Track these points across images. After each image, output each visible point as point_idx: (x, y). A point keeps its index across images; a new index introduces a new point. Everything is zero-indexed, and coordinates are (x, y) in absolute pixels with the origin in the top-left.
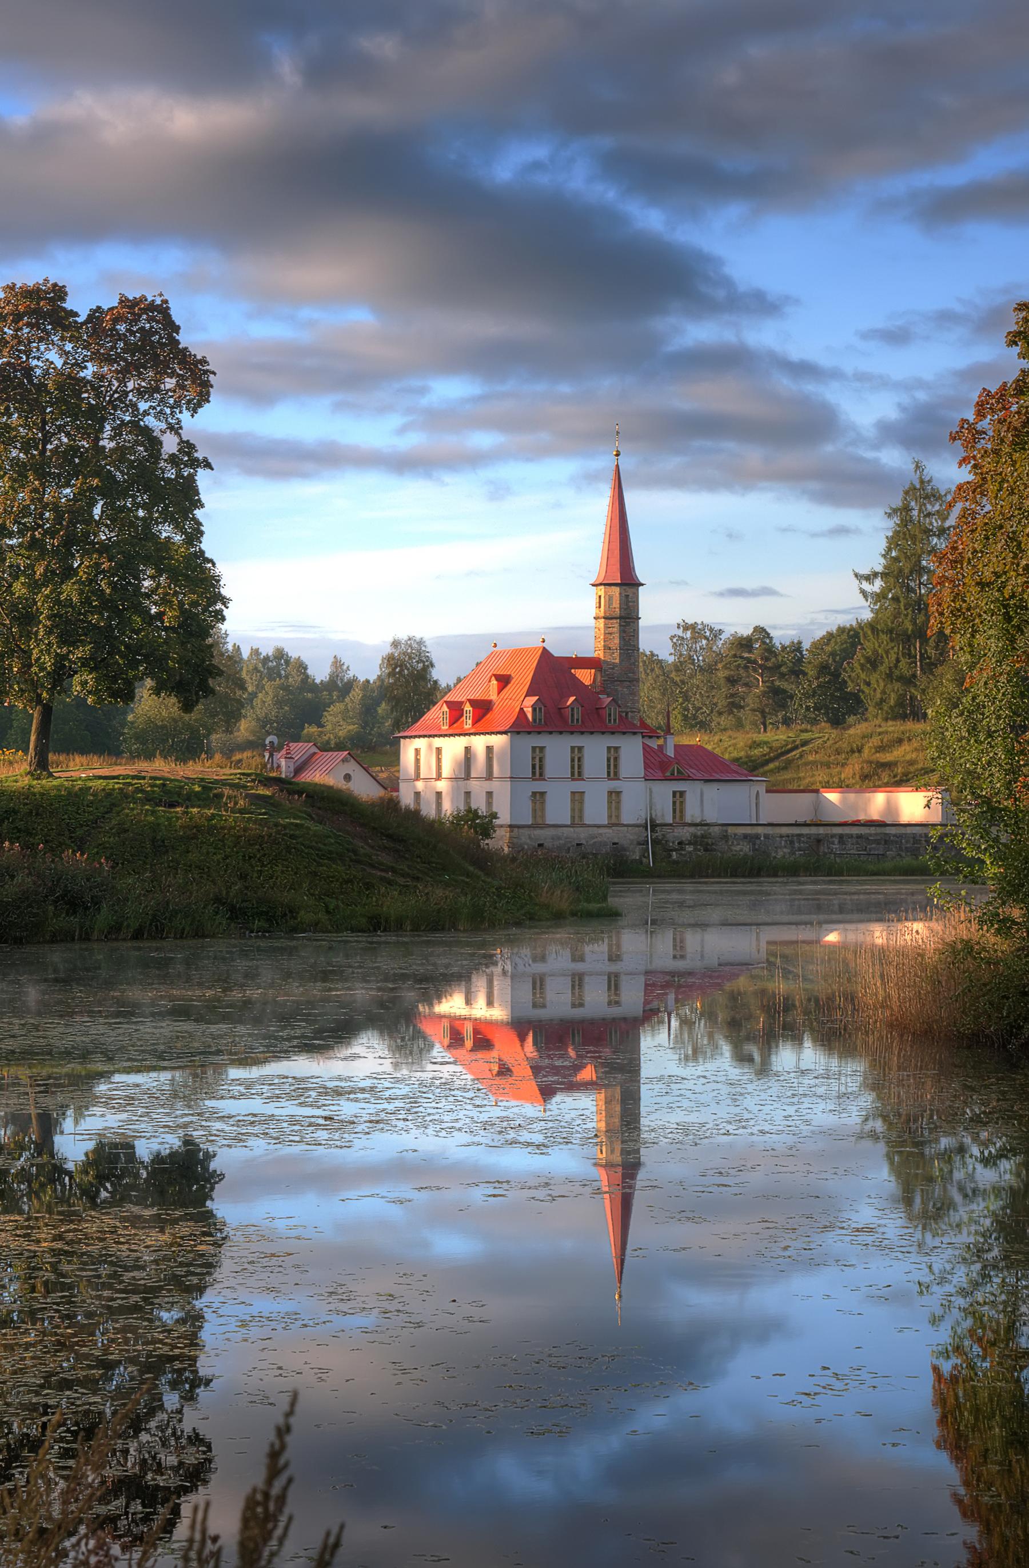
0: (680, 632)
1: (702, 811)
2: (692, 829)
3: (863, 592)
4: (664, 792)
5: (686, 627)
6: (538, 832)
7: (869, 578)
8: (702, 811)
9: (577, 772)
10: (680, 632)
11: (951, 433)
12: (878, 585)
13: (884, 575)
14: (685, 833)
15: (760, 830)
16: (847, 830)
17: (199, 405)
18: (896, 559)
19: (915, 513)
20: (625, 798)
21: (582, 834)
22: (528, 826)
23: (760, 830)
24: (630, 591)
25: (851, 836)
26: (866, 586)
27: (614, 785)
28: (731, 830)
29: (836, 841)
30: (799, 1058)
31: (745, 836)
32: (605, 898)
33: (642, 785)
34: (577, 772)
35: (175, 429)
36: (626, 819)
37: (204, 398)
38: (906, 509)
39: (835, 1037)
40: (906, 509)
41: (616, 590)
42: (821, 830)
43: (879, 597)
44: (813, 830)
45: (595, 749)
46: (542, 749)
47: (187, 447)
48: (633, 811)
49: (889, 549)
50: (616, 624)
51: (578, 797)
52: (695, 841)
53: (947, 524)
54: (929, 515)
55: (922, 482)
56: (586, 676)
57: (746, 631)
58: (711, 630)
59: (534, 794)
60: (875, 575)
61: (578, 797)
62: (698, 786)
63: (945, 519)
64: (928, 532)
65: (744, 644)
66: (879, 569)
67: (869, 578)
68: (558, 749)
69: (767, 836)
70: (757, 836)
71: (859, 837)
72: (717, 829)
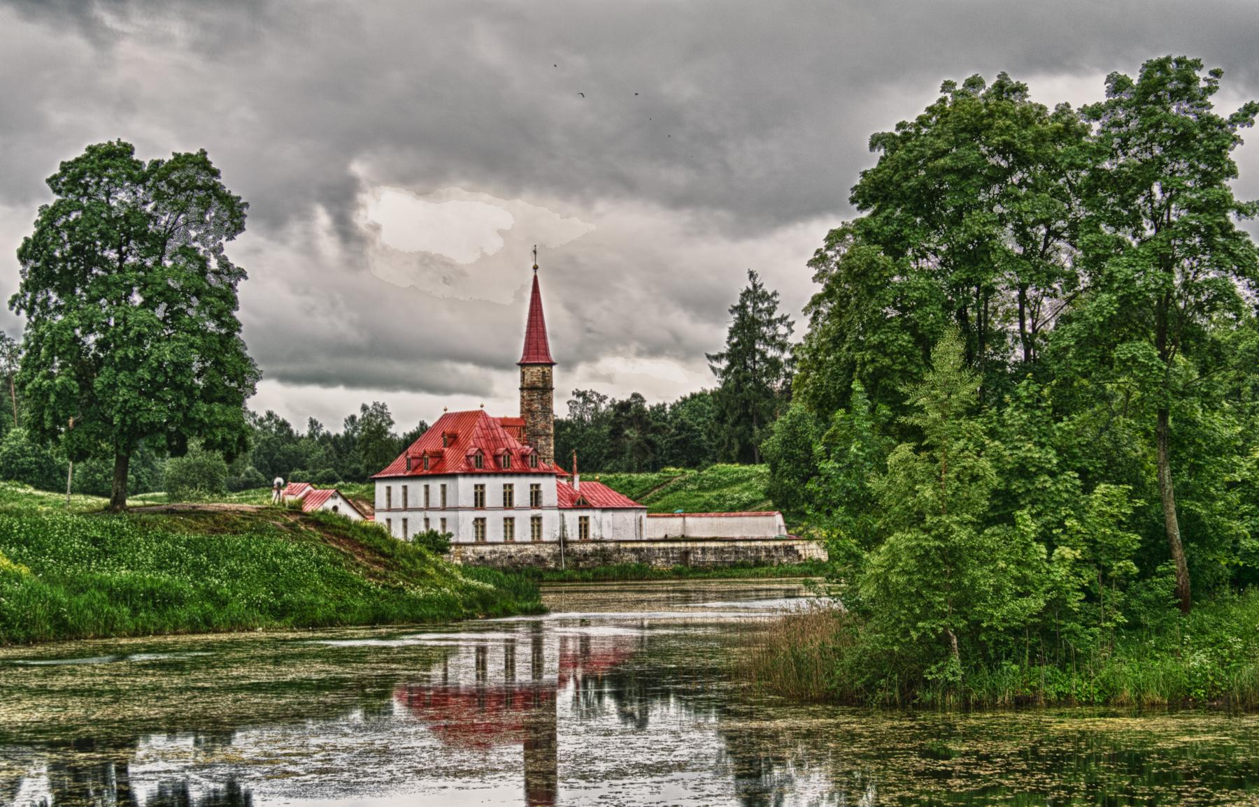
0: (574, 398)
1: (389, 500)
2: (593, 545)
3: (713, 369)
4: (573, 517)
5: (579, 394)
6: (479, 548)
7: (718, 358)
8: (389, 500)
9: (508, 501)
10: (574, 398)
11: (254, 393)
12: (724, 364)
13: (728, 356)
14: (589, 548)
15: (644, 545)
16: (708, 544)
17: (235, 232)
18: (735, 345)
19: (750, 310)
20: (544, 522)
21: (513, 549)
22: (472, 544)
23: (644, 545)
25: (710, 549)
26: (716, 364)
27: (536, 512)
28: (622, 545)
30: (666, 715)
32: (539, 598)
34: (508, 501)
35: (218, 251)
36: (545, 537)
37: (240, 228)
38: (743, 307)
39: (695, 701)
40: (743, 307)
42: (689, 545)
43: (725, 373)
44: (683, 545)
46: (482, 486)
47: (225, 265)
48: (550, 532)
49: (731, 338)
52: (595, 553)
53: (773, 317)
54: (761, 311)
55: (755, 286)
57: (625, 397)
58: (598, 395)
59: (476, 520)
60: (722, 356)
62: (598, 513)
63: (771, 314)
64: (760, 324)
65: (623, 407)
66: (724, 351)
67: (718, 358)
69: (649, 549)
70: (642, 549)
71: (716, 549)
72: (612, 545)
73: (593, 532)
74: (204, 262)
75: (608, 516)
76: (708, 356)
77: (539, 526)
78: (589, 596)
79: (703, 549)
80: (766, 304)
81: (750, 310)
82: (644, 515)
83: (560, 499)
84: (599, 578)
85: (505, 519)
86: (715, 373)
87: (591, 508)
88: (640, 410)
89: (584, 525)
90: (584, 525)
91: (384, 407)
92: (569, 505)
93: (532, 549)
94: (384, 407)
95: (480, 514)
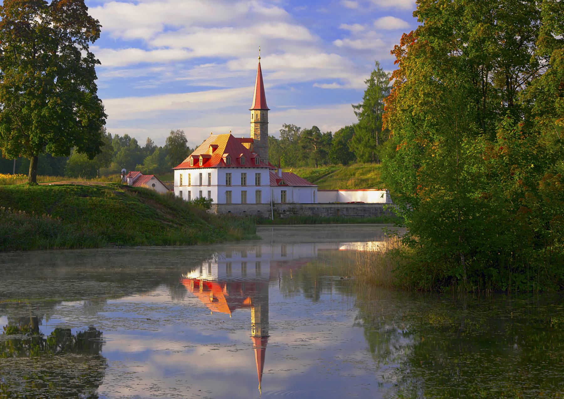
2: (289, 205)
3: (356, 113)
4: (278, 191)
5: (286, 127)
7: (358, 107)
12: (361, 110)
13: (364, 106)
14: (286, 207)
19: (376, 82)
23: (315, 206)
24: (264, 112)
26: (357, 110)
27: (258, 188)
28: (304, 206)
29: (345, 210)
31: (310, 208)
33: (269, 188)
38: (372, 80)
40: (372, 80)
41: (259, 112)
44: (336, 206)
45: (251, 174)
50: (259, 125)
51: (244, 193)
52: (290, 210)
53: (388, 86)
54: (382, 82)
55: (379, 70)
56: (247, 145)
57: (310, 128)
58: (296, 127)
60: (360, 106)
61: (244, 193)
62: (291, 188)
67: (358, 107)
68: (236, 174)
69: (318, 208)
70: (314, 208)
73: (289, 199)
74: (78, 54)
75: (296, 190)
76: (353, 106)
77: (260, 195)
78: (282, 232)
79: (347, 208)
80: (384, 79)
81: (376, 82)
82: (316, 189)
83: (271, 181)
84: (291, 222)
85: (242, 191)
86: (98, 60)
87: (287, 185)
88: (319, 135)
89: (283, 193)
90: (283, 193)
91: (182, 132)
92: (276, 184)
93: (257, 208)
94: (182, 132)
95: (229, 189)
